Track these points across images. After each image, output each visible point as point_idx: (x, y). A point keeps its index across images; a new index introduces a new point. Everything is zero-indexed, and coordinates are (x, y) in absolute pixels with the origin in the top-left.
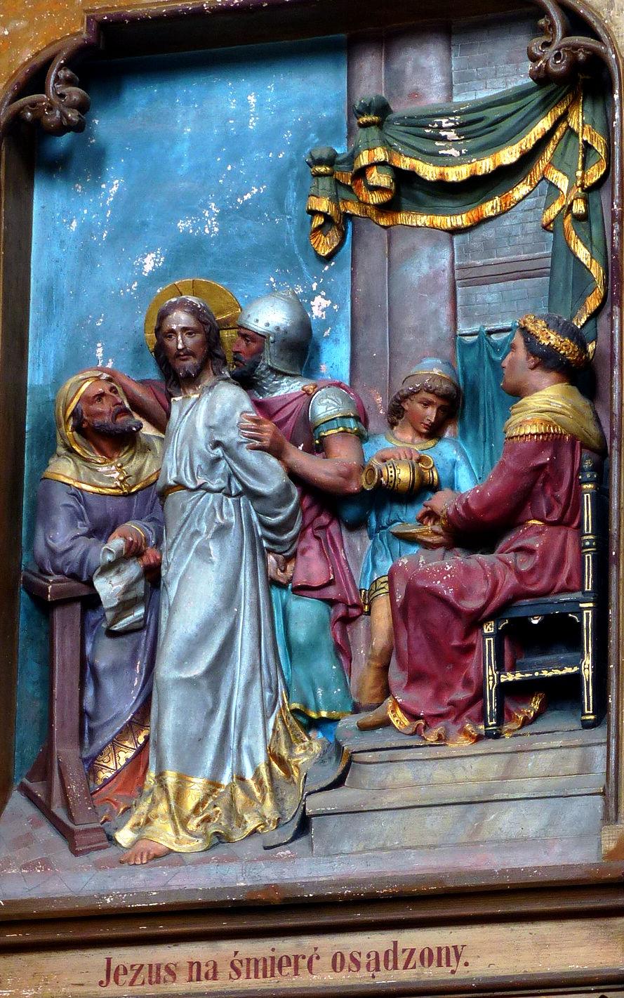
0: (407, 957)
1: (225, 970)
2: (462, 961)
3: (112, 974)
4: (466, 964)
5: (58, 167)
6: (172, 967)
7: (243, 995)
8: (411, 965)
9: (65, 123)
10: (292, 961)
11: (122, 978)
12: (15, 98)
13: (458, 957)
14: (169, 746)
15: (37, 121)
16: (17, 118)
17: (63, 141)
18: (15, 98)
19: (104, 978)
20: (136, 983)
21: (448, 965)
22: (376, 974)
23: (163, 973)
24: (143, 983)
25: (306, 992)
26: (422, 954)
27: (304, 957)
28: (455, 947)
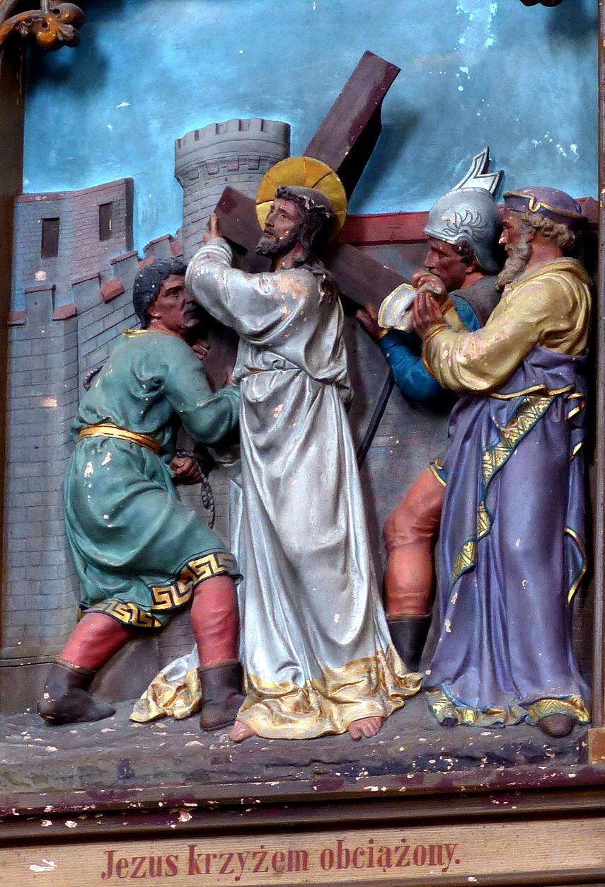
0: (223, 863)
1: (314, 860)
2: (453, 860)
3: (112, 868)
4: (458, 862)
5: (60, 77)
6: (172, 859)
7: (416, 883)
8: (404, 862)
9: (61, 38)
10: (286, 857)
11: (124, 871)
12: (10, 14)
13: (450, 856)
14: (535, 604)
15: (32, 36)
16: (13, 34)
17: (66, 54)
18: (10, 14)
19: (106, 870)
20: (138, 875)
21: (440, 863)
22: (388, 869)
23: (165, 866)
24: (267, 871)
25: (543, 876)
26: (416, 851)
27: (362, 853)
28: (447, 845)
